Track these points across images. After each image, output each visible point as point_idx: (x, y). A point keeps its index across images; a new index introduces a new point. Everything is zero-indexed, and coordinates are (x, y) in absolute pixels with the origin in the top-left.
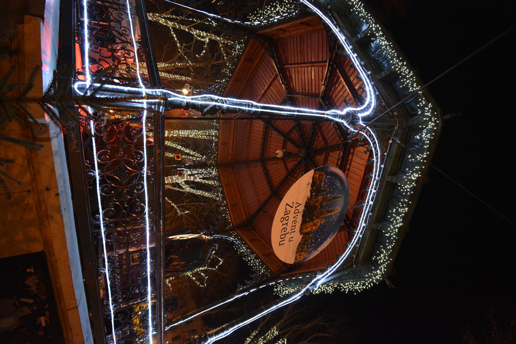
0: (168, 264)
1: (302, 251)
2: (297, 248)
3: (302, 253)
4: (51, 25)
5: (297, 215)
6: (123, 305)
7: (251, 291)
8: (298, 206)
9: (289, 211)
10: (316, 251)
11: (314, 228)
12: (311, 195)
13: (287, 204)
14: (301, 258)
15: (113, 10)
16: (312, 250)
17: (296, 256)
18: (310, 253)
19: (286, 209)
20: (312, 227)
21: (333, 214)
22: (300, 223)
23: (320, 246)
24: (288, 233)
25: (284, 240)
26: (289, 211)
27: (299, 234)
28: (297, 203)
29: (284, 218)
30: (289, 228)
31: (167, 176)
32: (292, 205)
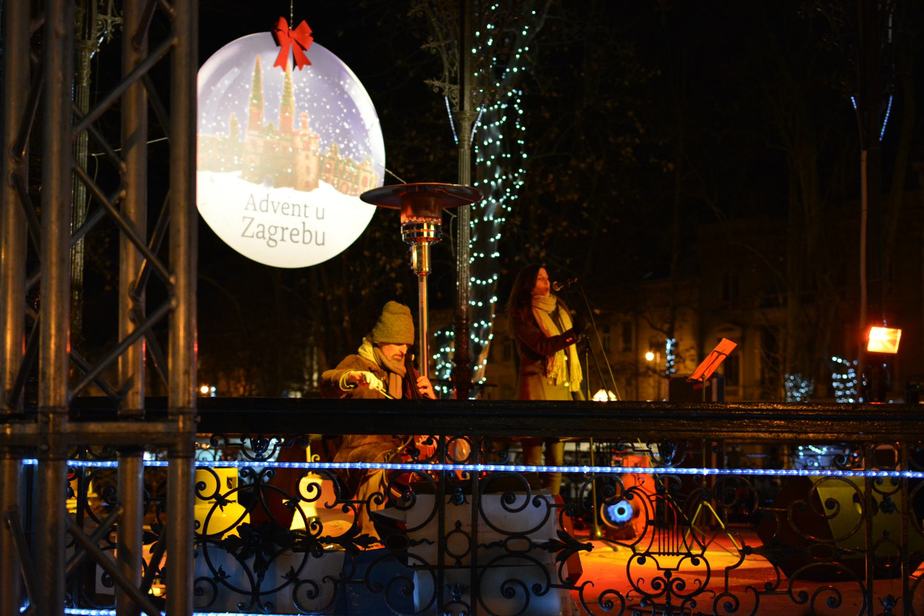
0: (163, 484)
1: (357, 177)
2: (346, 193)
3: (361, 178)
4: (57, 231)
5: (273, 202)
6: (593, 505)
7: (890, 31)
8: (254, 204)
9: (258, 226)
10: (370, 134)
11: (313, 147)
12: (238, 167)
13: (253, 219)
14: (371, 179)
15: (469, 603)
16: (364, 145)
18: (369, 152)
19: (252, 237)
20: (311, 154)
22: (290, 190)
23: (361, 119)
24: (304, 223)
25: (316, 233)
26: (258, 226)
27: (315, 191)
28: (246, 209)
29: (270, 239)
30: (294, 222)
31: (66, 504)
32: (248, 221)
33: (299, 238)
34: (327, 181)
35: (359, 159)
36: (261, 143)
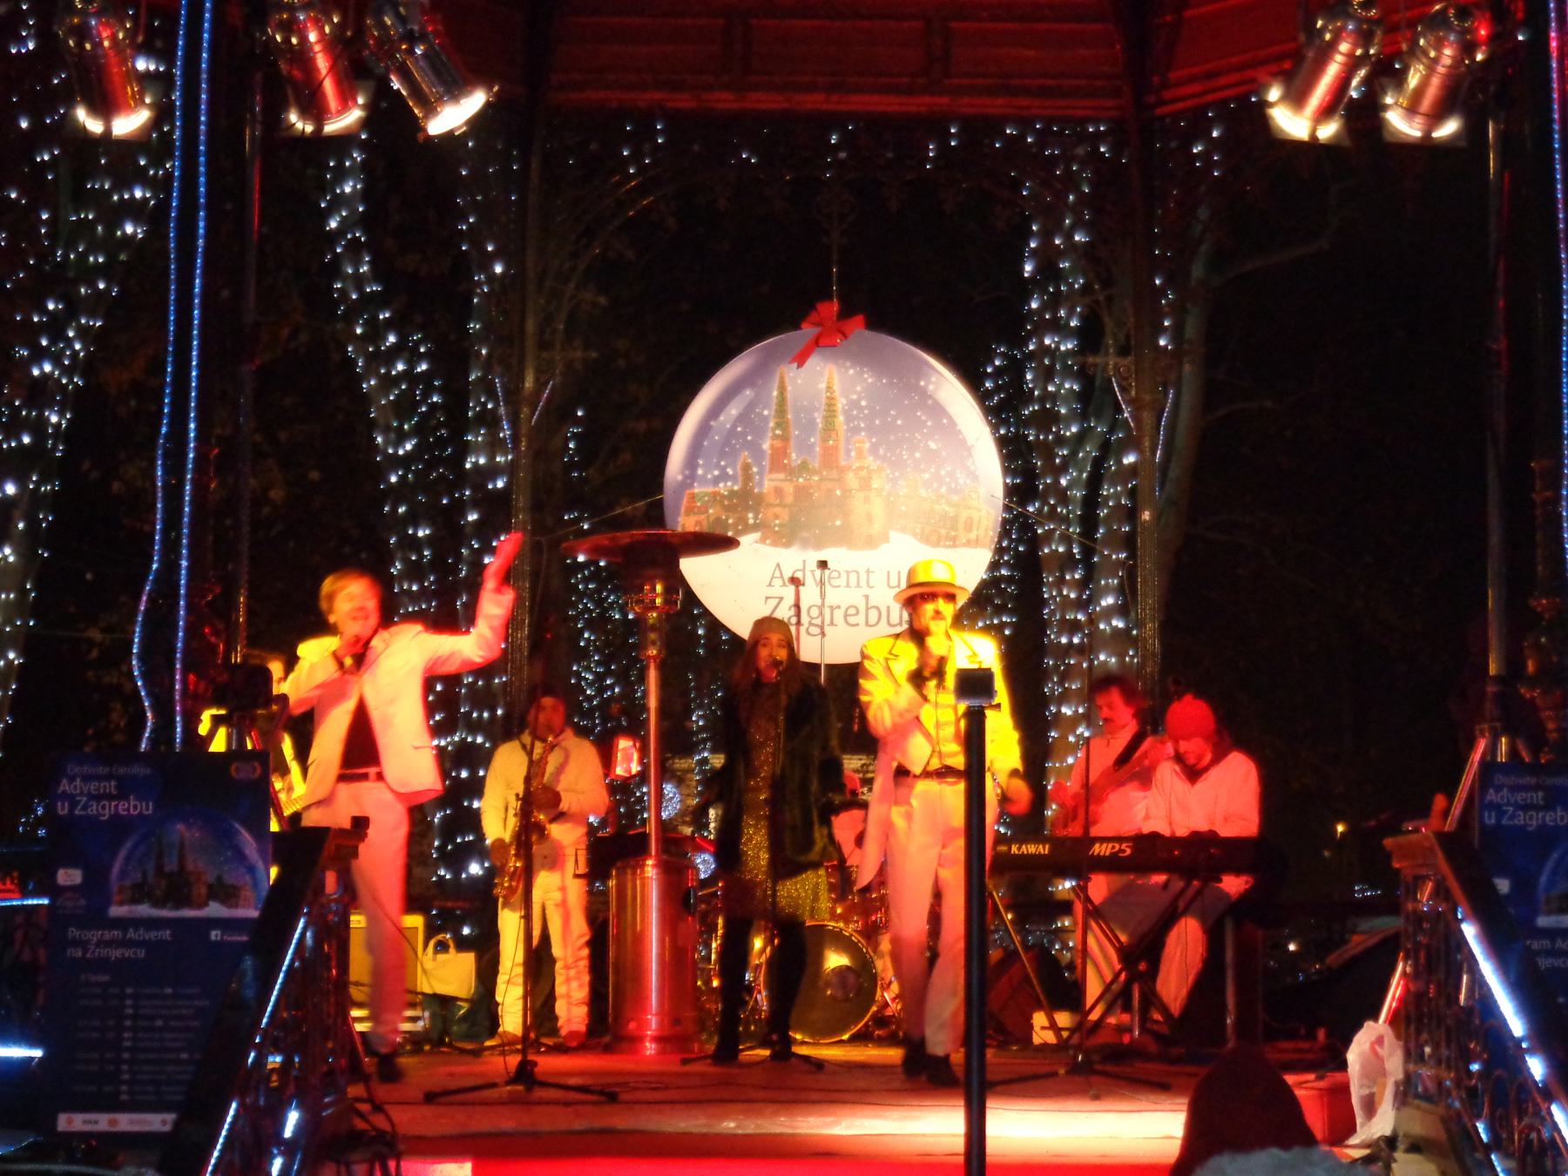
17: (969, 544)
21: (841, 403)
27: (884, 547)
33: (861, 619)
34: (903, 530)
35: (956, 491)
36: (789, 489)
